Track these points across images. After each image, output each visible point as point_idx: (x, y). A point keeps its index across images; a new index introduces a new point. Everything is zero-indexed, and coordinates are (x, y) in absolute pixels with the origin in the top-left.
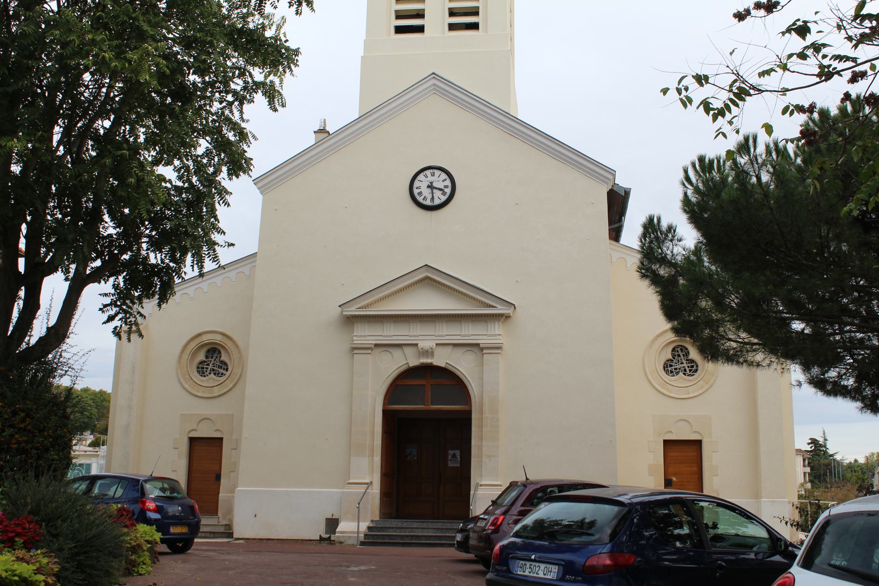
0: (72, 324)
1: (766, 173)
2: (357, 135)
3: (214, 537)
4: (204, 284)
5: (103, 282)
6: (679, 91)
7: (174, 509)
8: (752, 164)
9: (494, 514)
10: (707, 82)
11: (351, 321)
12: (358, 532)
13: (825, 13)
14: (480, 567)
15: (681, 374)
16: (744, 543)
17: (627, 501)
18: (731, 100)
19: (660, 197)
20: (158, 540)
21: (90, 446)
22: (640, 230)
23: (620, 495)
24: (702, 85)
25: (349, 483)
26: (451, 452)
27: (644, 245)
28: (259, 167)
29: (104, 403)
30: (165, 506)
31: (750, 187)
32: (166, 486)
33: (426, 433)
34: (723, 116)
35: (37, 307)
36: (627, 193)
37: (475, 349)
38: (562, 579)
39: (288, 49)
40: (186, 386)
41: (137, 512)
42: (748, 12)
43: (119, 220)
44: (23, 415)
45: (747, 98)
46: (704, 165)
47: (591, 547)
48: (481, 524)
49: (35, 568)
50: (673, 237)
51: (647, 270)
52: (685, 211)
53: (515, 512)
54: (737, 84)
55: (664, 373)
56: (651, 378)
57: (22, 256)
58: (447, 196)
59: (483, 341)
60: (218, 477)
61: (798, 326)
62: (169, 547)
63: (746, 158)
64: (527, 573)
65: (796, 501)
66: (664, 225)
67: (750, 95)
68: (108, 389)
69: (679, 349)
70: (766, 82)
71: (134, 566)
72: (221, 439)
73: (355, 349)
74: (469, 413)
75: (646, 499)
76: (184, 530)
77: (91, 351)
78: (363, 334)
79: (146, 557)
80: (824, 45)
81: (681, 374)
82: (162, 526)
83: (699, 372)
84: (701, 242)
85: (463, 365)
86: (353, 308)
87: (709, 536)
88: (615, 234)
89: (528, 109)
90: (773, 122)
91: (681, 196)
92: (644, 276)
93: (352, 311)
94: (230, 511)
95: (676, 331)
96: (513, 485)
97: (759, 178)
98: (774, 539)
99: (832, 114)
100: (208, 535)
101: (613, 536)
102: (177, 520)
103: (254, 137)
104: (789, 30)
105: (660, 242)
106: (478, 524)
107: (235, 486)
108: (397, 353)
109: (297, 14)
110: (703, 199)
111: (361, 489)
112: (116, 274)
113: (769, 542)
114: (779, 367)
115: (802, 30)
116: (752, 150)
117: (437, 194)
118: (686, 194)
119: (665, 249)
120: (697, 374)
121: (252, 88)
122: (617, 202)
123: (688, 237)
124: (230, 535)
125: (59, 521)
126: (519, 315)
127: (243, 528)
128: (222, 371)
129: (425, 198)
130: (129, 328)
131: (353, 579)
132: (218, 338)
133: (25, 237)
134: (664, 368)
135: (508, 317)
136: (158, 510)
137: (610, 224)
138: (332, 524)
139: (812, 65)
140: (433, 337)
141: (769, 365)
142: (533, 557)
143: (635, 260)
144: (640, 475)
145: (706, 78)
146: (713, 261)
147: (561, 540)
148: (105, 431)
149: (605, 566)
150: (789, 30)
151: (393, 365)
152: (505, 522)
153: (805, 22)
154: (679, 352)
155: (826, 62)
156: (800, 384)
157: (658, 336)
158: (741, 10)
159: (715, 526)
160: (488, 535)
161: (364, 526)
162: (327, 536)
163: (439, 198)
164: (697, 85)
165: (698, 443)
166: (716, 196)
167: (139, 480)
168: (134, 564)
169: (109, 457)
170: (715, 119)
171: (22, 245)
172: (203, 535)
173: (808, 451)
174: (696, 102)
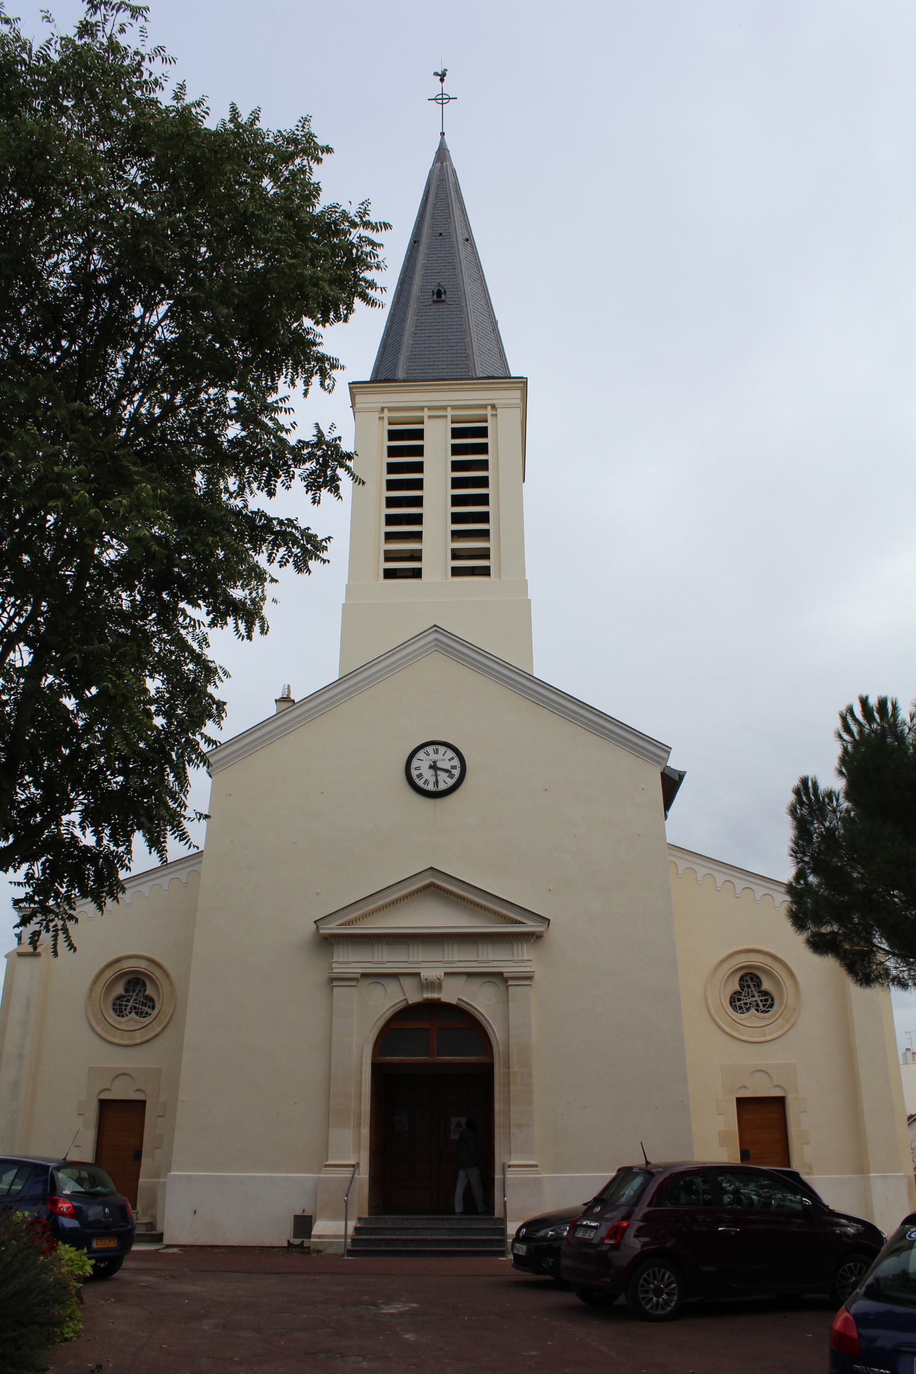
2: (338, 700)
5: (11, 870)
7: (94, 1212)
11: (328, 942)
12: (346, 1236)
15: (753, 1010)
25: (326, 1166)
26: (454, 1120)
30: (84, 1207)
32: (84, 1174)
33: (434, 1093)
40: (97, 1029)
53: (639, 1217)
56: (715, 1016)
58: (454, 780)
59: (508, 969)
60: (138, 1156)
69: (748, 978)
72: (143, 1102)
73: (334, 980)
74: (490, 1067)
76: (111, 1243)
78: (345, 960)
81: (753, 1010)
83: (775, 1007)
85: (482, 1001)
86: (333, 925)
93: (331, 928)
94: (152, 1203)
96: (625, 1174)
111: (346, 1174)
112: (31, 858)
117: (443, 776)
120: (773, 1011)
124: (159, 1238)
126: (554, 933)
128: (146, 1009)
129: (426, 782)
132: (142, 965)
134: (731, 1003)
136: (75, 1213)
138: (303, 1224)
140: (441, 964)
151: (384, 1002)
161: (352, 1224)
163: (445, 782)
167: (49, 1167)
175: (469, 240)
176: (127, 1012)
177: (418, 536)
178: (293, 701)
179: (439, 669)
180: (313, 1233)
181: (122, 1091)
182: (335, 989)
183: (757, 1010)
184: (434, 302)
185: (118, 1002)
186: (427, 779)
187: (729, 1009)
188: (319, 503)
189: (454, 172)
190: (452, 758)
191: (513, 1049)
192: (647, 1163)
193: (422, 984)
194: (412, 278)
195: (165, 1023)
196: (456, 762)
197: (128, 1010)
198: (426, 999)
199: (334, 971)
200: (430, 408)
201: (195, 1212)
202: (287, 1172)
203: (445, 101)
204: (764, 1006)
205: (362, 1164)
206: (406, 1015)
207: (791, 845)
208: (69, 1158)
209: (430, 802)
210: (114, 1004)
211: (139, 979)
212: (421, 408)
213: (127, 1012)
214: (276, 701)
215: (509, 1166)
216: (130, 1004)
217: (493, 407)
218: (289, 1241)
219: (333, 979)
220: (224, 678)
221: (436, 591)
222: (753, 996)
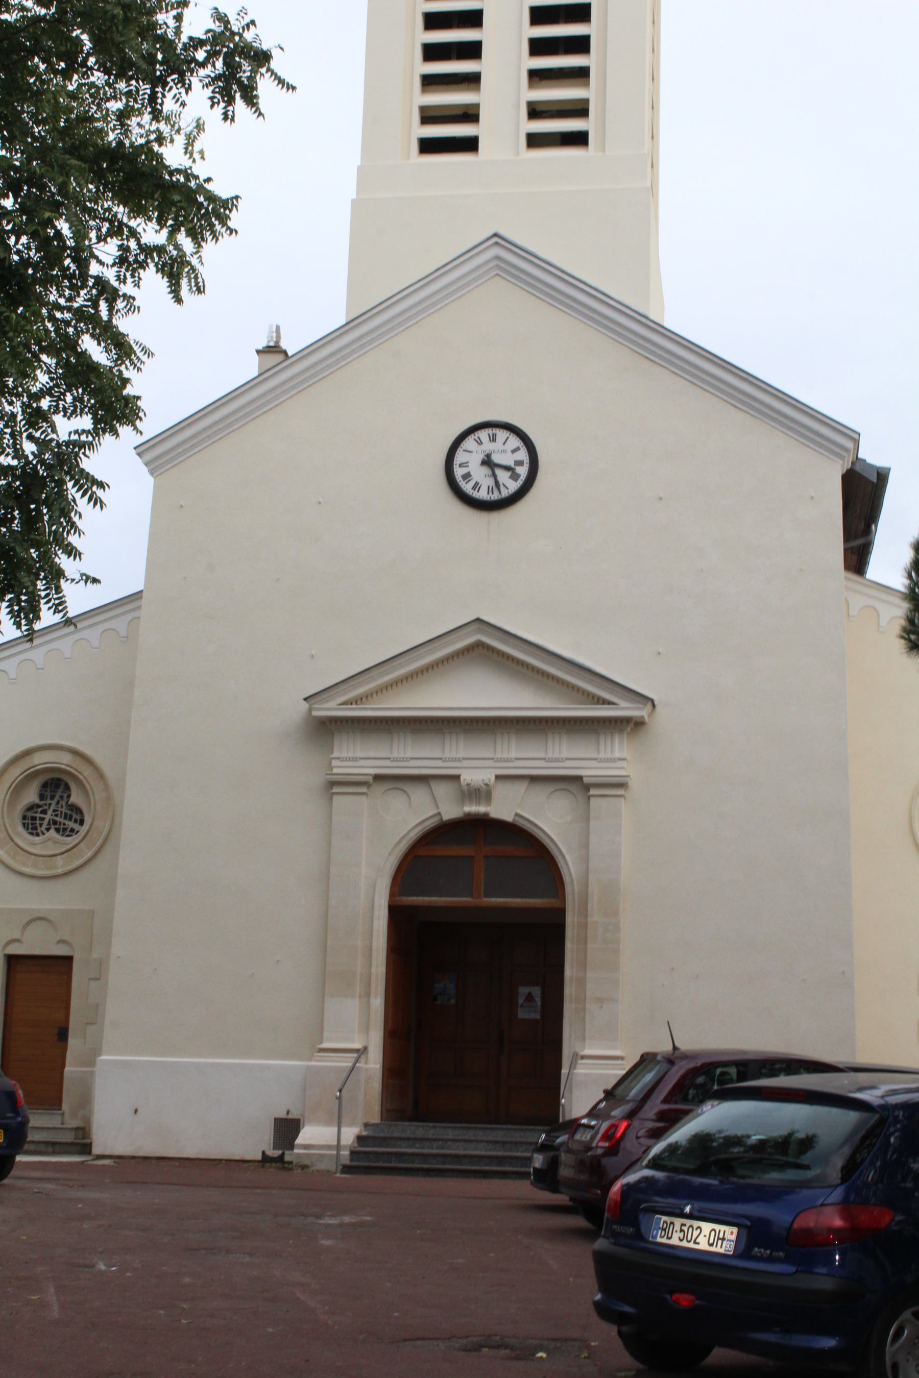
9: (608, 1117)
11: (326, 729)
12: (338, 1147)
14: (580, 1222)
23: (861, 1089)
26: (523, 991)
28: (153, 423)
33: (475, 948)
36: (882, 476)
37: (573, 788)
38: (744, 1250)
39: (211, 198)
47: (806, 1192)
48: (583, 1136)
58: (520, 482)
59: (589, 771)
60: (63, 1034)
64: (675, 1241)
72: (69, 959)
73: (334, 785)
74: (560, 913)
78: (351, 755)
85: (549, 818)
88: (857, 558)
89: (682, 310)
93: (331, 708)
94: (86, 1101)
96: (646, 1060)
100: (42, 1148)
101: (849, 1170)
103: (145, 350)
106: (578, 1137)
107: (96, 1052)
111: (345, 1062)
124: (86, 1148)
126: (663, 721)
128: (71, 824)
132: (64, 760)
142: (688, 1209)
147: (744, 1177)
149: (832, 1230)
151: (407, 817)
152: (631, 1135)
161: (350, 1134)
162: (278, 1153)
172: (32, 1147)
176: (43, 828)
178: (285, 352)
179: (501, 306)
180: (299, 1141)
182: (335, 797)
185: (30, 814)
188: (233, 120)
190: (517, 449)
191: (594, 890)
192: (675, 1048)
193: (463, 792)
195: (99, 843)
196: (523, 455)
197: (45, 826)
198: (469, 814)
199: (335, 771)
201: (136, 1111)
205: (371, 1049)
206: (441, 834)
207: (903, 622)
210: (24, 818)
211: (59, 780)
213: (43, 828)
214: (258, 352)
215: (583, 1057)
216: (48, 817)
218: (263, 1153)
219: (333, 784)
220: (144, 358)
221: (505, 171)
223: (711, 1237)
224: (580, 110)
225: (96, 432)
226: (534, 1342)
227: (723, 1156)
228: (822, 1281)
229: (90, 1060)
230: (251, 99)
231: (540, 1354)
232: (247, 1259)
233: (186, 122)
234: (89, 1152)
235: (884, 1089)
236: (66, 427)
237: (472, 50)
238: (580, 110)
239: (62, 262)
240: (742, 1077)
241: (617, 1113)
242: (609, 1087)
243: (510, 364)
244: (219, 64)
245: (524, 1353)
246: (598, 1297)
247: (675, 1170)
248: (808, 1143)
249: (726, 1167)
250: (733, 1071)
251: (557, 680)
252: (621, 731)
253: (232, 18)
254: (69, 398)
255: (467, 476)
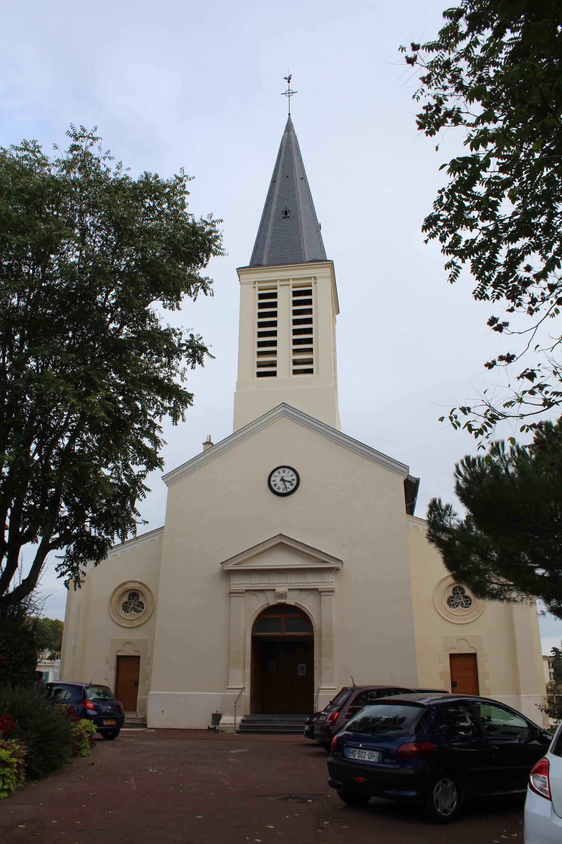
0: (39, 578)
1: (512, 467)
2: (232, 445)
3: (134, 727)
4: (128, 549)
5: (60, 548)
6: (451, 418)
7: (107, 708)
8: (502, 461)
9: (331, 711)
10: (469, 411)
11: (228, 574)
12: (235, 724)
13: (545, 363)
14: (322, 750)
15: (460, 606)
16: (511, 731)
17: (426, 704)
18: (487, 423)
19: (440, 486)
20: (95, 731)
21: (48, 659)
22: (427, 509)
23: (420, 699)
24: (466, 414)
26: (300, 665)
27: (431, 519)
28: (168, 468)
29: (58, 629)
30: (100, 705)
31: (501, 477)
32: (101, 691)
33: (282, 650)
34: (482, 434)
35: (16, 566)
36: (417, 481)
37: (315, 592)
38: (381, 761)
40: (115, 619)
41: (80, 710)
42: (494, 363)
43: (73, 507)
44: (4, 641)
45: (497, 421)
46: (469, 462)
47: (403, 738)
48: (322, 719)
49: (10, 753)
50: (450, 513)
51: (434, 536)
52: (458, 494)
53: (347, 710)
54: (490, 412)
55: (447, 606)
56: (439, 610)
57: (7, 529)
58: (294, 486)
59: (321, 587)
60: (137, 684)
61: (540, 572)
62: (102, 735)
63: (498, 457)
64: (356, 757)
65: (545, 694)
66: (444, 505)
67: (500, 420)
68: (62, 619)
70: (508, 411)
71: (78, 750)
72: (139, 657)
74: (312, 637)
75: (441, 701)
76: (113, 723)
77: (51, 597)
79: (86, 743)
80: (546, 385)
81: (460, 606)
82: (97, 720)
84: (470, 515)
85: (307, 604)
86: (230, 565)
87: (485, 727)
88: (410, 509)
89: (348, 425)
90: (516, 433)
91: (454, 484)
92: (431, 541)
93: (230, 566)
94: (145, 708)
95: (455, 577)
96: (344, 690)
97: (507, 470)
98: (532, 727)
99: (554, 425)
100: (130, 725)
101: (418, 729)
102: (109, 716)
103: (164, 442)
104: (522, 376)
105: (441, 517)
106: (320, 719)
107: (149, 690)
108: (261, 596)
109: (192, 368)
110: (470, 486)
111: (237, 693)
112: (69, 543)
113: (528, 731)
114: (529, 602)
115: (531, 376)
116: (501, 451)
117: (288, 484)
118: (458, 483)
119: (445, 521)
120: (471, 606)
121: (162, 413)
122: (411, 488)
123: (461, 512)
124: (145, 726)
125: (28, 719)
126: (346, 568)
127: (156, 720)
128: (139, 609)
129: (279, 488)
130: (76, 581)
131: (232, 760)
132: (137, 586)
133: (9, 518)
135: (337, 569)
136: (95, 708)
137: (406, 503)
139: (539, 398)
141: (522, 601)
142: (361, 746)
143: (424, 529)
144: (433, 677)
145: (469, 409)
146: (479, 528)
147: (380, 733)
148: (59, 648)
149: (412, 752)
150: (522, 376)
151: (258, 604)
152: (339, 718)
153: (532, 370)
154: (457, 591)
155: (548, 396)
156: (543, 613)
157: (443, 580)
158: (490, 361)
159: (489, 719)
160: (328, 727)
161: (239, 719)
162: (213, 726)
164: (463, 414)
165: (474, 656)
166: (477, 482)
167: (82, 687)
168: (79, 749)
169: (62, 668)
170: (476, 436)
171: (8, 522)
172: (126, 725)
173: (551, 657)
174: (463, 425)
175: (304, 178)
177: (274, 353)
178: (212, 444)
180: (220, 722)
181: (128, 651)
183: (462, 606)
184: (284, 218)
185: (125, 605)
186: (280, 487)
187: (447, 606)
189: (296, 137)
192: (354, 685)
193: (276, 595)
194: (271, 203)
196: (294, 477)
198: (279, 603)
200: (281, 280)
202: (209, 692)
203: (290, 94)
204: (466, 604)
205: (246, 688)
206: (269, 610)
207: (427, 532)
208: (92, 683)
209: (281, 499)
210: (123, 606)
212: (276, 281)
214: (203, 444)
215: (321, 689)
217: (315, 278)
219: (231, 593)
221: (286, 384)
222: (460, 599)
223: (368, 756)
224: (310, 362)
225: (146, 471)
226: (307, 796)
227: (372, 726)
228: (410, 770)
229: (146, 693)
230: (201, 362)
231: (309, 801)
232: (203, 767)
233: (180, 368)
234: (146, 727)
235: (429, 699)
236: (137, 469)
237: (274, 343)
238: (310, 362)
239: (139, 415)
240: (379, 696)
241: (334, 709)
242: (331, 700)
243: (290, 446)
244: (190, 351)
245: (303, 800)
246: (330, 779)
247: (355, 731)
248: (402, 720)
249: (374, 730)
250: (375, 693)
251: (305, 553)
252: (331, 572)
253: (195, 336)
254: (138, 459)
255: (275, 485)
